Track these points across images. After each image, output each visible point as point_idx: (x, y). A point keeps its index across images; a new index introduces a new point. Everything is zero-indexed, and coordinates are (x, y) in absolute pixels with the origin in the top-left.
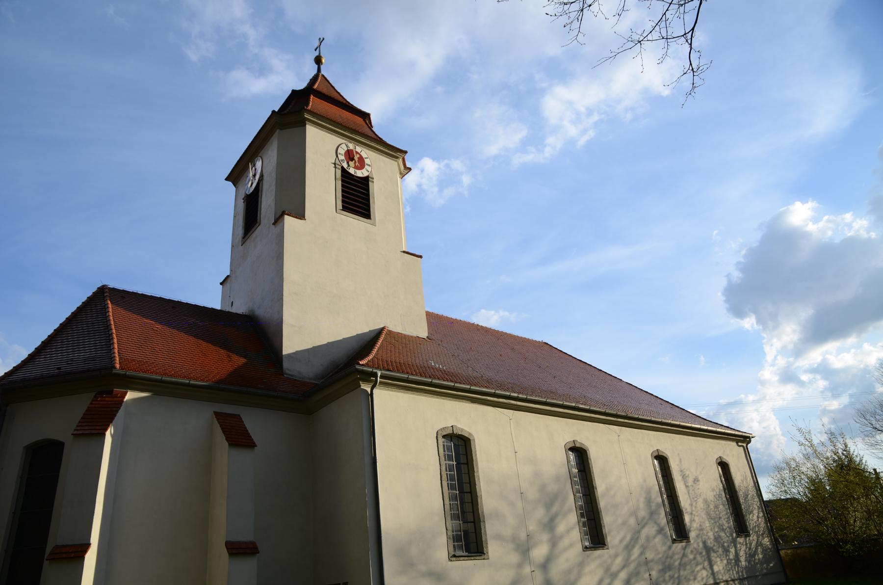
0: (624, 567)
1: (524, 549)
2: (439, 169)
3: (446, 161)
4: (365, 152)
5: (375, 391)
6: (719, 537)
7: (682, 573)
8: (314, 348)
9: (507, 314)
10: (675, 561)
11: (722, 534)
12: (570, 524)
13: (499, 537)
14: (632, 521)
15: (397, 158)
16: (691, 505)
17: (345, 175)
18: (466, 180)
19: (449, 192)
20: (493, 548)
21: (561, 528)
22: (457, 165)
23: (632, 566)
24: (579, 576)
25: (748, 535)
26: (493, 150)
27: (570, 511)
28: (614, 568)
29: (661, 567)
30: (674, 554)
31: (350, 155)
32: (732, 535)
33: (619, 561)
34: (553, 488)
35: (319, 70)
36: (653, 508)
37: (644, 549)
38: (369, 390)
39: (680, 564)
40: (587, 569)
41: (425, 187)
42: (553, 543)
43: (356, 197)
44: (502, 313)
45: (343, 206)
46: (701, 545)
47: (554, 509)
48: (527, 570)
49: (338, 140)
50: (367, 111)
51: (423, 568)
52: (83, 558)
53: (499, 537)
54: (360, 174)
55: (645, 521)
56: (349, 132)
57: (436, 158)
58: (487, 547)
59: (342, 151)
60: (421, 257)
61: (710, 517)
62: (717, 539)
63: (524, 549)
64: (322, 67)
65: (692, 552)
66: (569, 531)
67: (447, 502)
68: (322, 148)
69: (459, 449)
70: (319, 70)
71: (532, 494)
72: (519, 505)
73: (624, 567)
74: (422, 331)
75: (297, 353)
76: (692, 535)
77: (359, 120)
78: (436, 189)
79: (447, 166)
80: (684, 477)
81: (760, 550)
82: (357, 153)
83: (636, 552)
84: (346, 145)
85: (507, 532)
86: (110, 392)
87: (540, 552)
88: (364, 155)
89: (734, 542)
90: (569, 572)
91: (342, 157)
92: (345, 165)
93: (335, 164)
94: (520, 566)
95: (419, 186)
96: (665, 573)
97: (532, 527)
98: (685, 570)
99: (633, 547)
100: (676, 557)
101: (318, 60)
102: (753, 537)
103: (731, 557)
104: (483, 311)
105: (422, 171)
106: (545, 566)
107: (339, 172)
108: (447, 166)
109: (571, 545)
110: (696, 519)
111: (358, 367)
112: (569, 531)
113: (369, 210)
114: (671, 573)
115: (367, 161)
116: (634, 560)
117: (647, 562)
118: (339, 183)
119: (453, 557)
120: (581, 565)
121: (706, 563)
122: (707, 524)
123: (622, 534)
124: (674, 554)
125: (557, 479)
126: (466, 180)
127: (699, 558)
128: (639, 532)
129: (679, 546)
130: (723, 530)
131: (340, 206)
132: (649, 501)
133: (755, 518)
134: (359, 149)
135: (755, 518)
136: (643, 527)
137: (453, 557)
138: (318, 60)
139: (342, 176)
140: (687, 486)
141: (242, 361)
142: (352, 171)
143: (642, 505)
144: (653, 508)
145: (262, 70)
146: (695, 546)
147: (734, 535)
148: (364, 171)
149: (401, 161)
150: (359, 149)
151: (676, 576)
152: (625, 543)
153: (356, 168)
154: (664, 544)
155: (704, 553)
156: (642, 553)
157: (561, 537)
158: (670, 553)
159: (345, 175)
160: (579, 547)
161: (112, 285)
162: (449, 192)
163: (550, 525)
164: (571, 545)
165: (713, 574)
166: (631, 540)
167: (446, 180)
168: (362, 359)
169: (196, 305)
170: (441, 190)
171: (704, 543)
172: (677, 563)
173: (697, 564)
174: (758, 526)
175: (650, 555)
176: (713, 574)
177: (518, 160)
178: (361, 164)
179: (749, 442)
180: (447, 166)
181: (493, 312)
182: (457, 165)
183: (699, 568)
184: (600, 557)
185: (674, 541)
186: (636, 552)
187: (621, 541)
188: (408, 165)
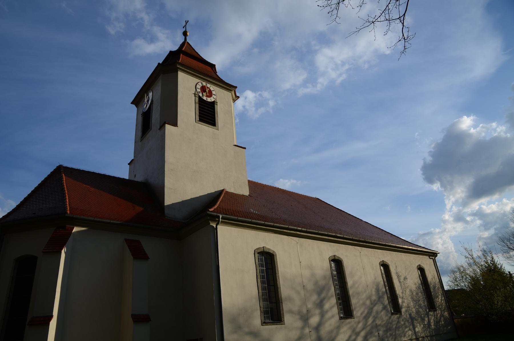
0: (363, 329)
1: (305, 318)
2: (255, 97)
3: (260, 92)
4: (212, 87)
7: (397, 332)
9: (295, 181)
11: (421, 310)
12: (332, 304)
13: (291, 312)
14: (368, 302)
15: (231, 90)
17: (200, 98)
18: (271, 103)
19: (262, 110)
20: (287, 318)
21: (327, 306)
22: (266, 94)
24: (337, 334)
26: (287, 86)
27: (332, 296)
28: (358, 330)
29: (385, 329)
30: (392, 321)
31: (203, 89)
32: (426, 310)
33: (360, 325)
34: (322, 283)
35: (185, 39)
38: (215, 226)
39: (396, 327)
41: (247, 107)
42: (322, 315)
43: (207, 114)
44: (292, 181)
45: (200, 119)
46: (408, 316)
47: (323, 295)
48: (307, 330)
49: (197, 80)
50: (214, 63)
51: (246, 330)
53: (291, 312)
54: (209, 100)
56: (203, 75)
57: (254, 90)
58: (284, 318)
59: (199, 86)
60: (245, 148)
61: (413, 300)
62: (418, 312)
63: (305, 318)
64: (187, 37)
65: (403, 320)
66: (331, 308)
68: (187, 85)
69: (267, 261)
70: (185, 39)
71: (310, 286)
72: (302, 292)
73: (363, 329)
74: (245, 191)
76: (403, 310)
77: (209, 68)
78: (254, 109)
80: (398, 277)
81: (442, 319)
82: (208, 88)
83: (370, 320)
85: (295, 309)
87: (314, 320)
88: (212, 89)
89: (427, 314)
90: (331, 332)
91: (199, 90)
92: (201, 95)
93: (195, 94)
94: (303, 328)
95: (244, 107)
97: (310, 305)
99: (369, 317)
100: (394, 323)
101: (185, 34)
102: (439, 312)
104: (281, 180)
105: (246, 98)
106: (317, 328)
107: (197, 99)
108: (260, 95)
109: (333, 316)
110: (406, 301)
111: (208, 212)
112: (331, 308)
114: (391, 332)
115: (214, 93)
117: (377, 326)
118: (197, 105)
119: (264, 323)
120: (338, 328)
123: (362, 309)
125: (325, 277)
126: (271, 103)
127: (407, 324)
128: (372, 308)
130: (421, 307)
131: (198, 119)
132: (378, 290)
133: (440, 300)
134: (209, 85)
135: (440, 300)
137: (264, 323)
139: (199, 101)
140: (400, 282)
141: (141, 209)
142: (205, 98)
146: (405, 316)
148: (212, 98)
149: (233, 92)
150: (209, 85)
152: (364, 315)
153: (207, 96)
154: (387, 315)
156: (374, 321)
157: (327, 312)
159: (201, 103)
160: (337, 317)
162: (262, 110)
163: (320, 305)
164: (333, 316)
165: (415, 333)
166: (368, 313)
167: (260, 103)
170: (257, 109)
172: (394, 327)
173: (406, 327)
174: (442, 305)
175: (378, 322)
177: (302, 92)
178: (210, 94)
179: (436, 256)
180: (260, 95)
181: (287, 181)
182: (266, 94)
183: (407, 330)
184: (349, 323)
185: (392, 314)
186: (370, 320)
187: (361, 314)
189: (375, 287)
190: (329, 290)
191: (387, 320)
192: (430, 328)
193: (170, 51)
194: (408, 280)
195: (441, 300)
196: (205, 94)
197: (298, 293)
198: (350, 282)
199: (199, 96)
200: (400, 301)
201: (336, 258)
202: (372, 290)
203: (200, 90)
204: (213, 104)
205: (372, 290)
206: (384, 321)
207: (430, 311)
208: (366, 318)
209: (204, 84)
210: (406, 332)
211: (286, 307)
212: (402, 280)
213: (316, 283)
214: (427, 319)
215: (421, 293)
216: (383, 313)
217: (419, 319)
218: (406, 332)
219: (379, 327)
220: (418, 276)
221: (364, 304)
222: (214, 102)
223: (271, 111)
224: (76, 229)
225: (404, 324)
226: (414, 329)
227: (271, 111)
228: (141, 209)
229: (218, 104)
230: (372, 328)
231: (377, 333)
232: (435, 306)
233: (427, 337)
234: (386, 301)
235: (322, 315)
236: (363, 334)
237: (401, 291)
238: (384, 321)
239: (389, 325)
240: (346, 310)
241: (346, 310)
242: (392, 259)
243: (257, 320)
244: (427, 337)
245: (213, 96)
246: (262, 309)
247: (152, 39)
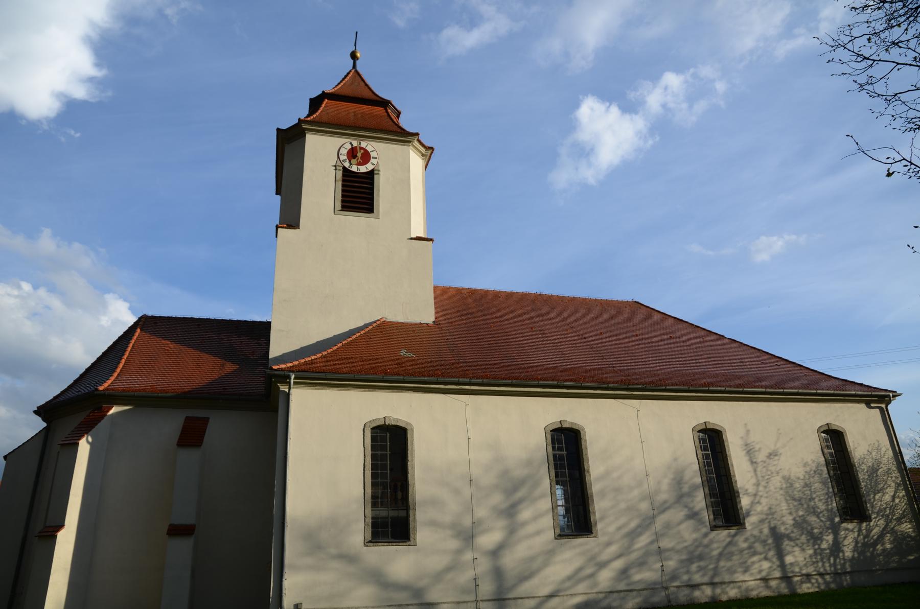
0: (619, 556)
1: (467, 536)
2: (686, 82)
3: (692, 70)
5: (292, 391)
6: (805, 521)
7: (722, 564)
8: (302, 348)
9: (794, 237)
10: (712, 550)
11: (812, 519)
12: (543, 508)
13: (433, 524)
14: (644, 506)
15: (409, 142)
18: (721, 87)
19: (701, 106)
20: (422, 534)
21: (525, 514)
22: (706, 71)
23: (634, 556)
24: (546, 564)
26: (748, 43)
27: (542, 496)
29: (684, 557)
30: (711, 542)
32: (832, 520)
33: (613, 549)
34: (519, 473)
37: (658, 537)
38: (287, 390)
39: (721, 554)
40: (558, 558)
42: (512, 531)
43: (358, 193)
44: (787, 237)
46: (766, 531)
47: (519, 495)
48: (468, 556)
51: (333, 551)
53: (433, 524)
54: (363, 169)
55: (668, 505)
56: (351, 130)
58: (415, 534)
59: (344, 151)
60: (431, 240)
62: (800, 524)
64: (357, 62)
65: (746, 540)
68: (323, 155)
72: (467, 492)
77: (379, 110)
78: (685, 106)
79: (694, 76)
80: (750, 452)
81: (888, 537)
83: (643, 540)
84: (343, 144)
85: (447, 519)
86: (100, 409)
87: (489, 539)
88: (369, 149)
89: (835, 530)
90: (532, 559)
91: (343, 158)
92: (347, 165)
94: (459, 552)
95: (664, 106)
96: (692, 563)
97: (481, 512)
98: (729, 559)
99: (640, 534)
100: (715, 545)
101: (353, 56)
102: (877, 525)
103: (824, 545)
104: (763, 238)
105: (666, 88)
106: (495, 553)
107: (340, 173)
109: (538, 533)
110: (764, 501)
113: (372, 204)
114: (702, 564)
115: (372, 154)
116: (638, 549)
117: (660, 551)
118: (340, 184)
119: (367, 543)
120: (550, 554)
121: (771, 554)
122: (784, 506)
123: (623, 520)
124: (711, 542)
125: (529, 463)
126: (721, 87)
127: (758, 547)
128: (653, 518)
132: (678, 481)
133: (887, 498)
134: (363, 144)
135: (888, 496)
136: (664, 511)
137: (367, 543)
138: (353, 56)
139: (343, 175)
142: (354, 168)
143: (665, 486)
144: (686, 489)
145: (472, 21)
146: (756, 532)
147: (837, 519)
149: (416, 143)
151: (711, 566)
152: (626, 530)
153: (359, 164)
154: (696, 530)
155: (770, 541)
157: (524, 524)
158: (706, 541)
160: (551, 534)
161: (151, 313)
162: (701, 106)
163: (510, 512)
164: (538, 533)
165: (782, 566)
166: (639, 526)
168: (101, 385)
169: (230, 321)
170: (691, 107)
171: (773, 530)
172: (715, 553)
173: (755, 553)
174: (893, 508)
175: (665, 543)
176: (782, 566)
177: (783, 49)
178: (366, 157)
179: (889, 402)
181: (775, 238)
182: (706, 71)
183: (755, 558)
184: (581, 545)
185: (714, 528)
186: (643, 540)
187: (619, 529)
188: (428, 144)
193: (311, 100)
196: (354, 161)
197: (457, 492)
199: (344, 168)
202: (659, 483)
203: (345, 157)
204: (370, 176)
205: (659, 483)
209: (355, 144)
210: (753, 563)
211: (421, 516)
213: (505, 473)
214: (830, 538)
215: (824, 483)
216: (683, 526)
217: (803, 538)
218: (753, 563)
219: (667, 554)
221: (629, 509)
222: (373, 171)
224: (114, 410)
225: (750, 547)
228: (235, 367)
229: (381, 173)
230: (647, 554)
231: (658, 565)
232: (866, 509)
233: (821, 575)
234: (700, 501)
235: (512, 531)
236: (618, 564)
237: (754, 481)
238: (685, 541)
239: (700, 549)
240: (578, 519)
241: (578, 519)
242: (733, 418)
244: (821, 575)
245: (372, 160)
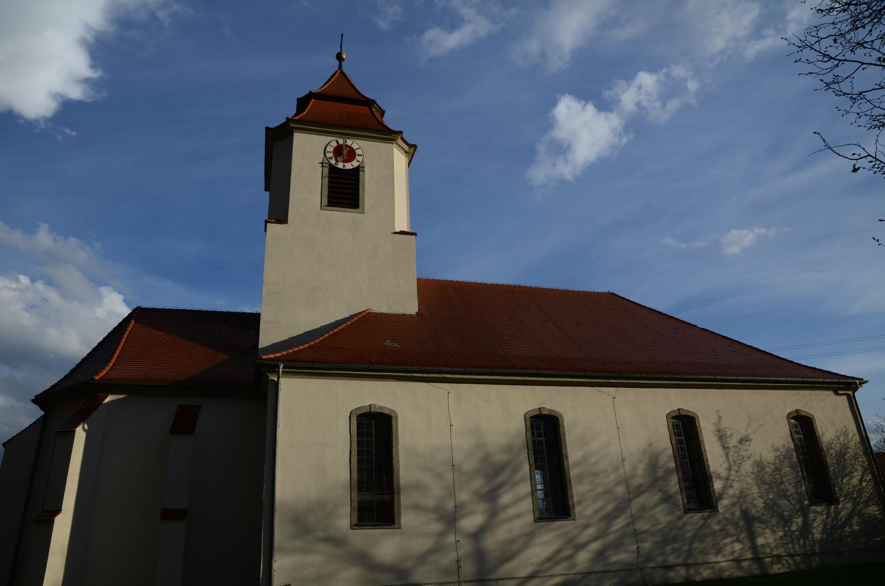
0: (596, 538)
1: (450, 519)
2: (659, 81)
3: (665, 70)
4: (353, 143)
6: (775, 504)
7: (696, 545)
8: (290, 338)
9: (763, 231)
11: (783, 502)
12: (521, 496)
14: (620, 490)
15: (393, 140)
16: (729, 469)
17: (333, 169)
18: (692, 86)
19: (674, 104)
20: (407, 518)
21: (506, 498)
22: (679, 71)
23: (611, 538)
24: (525, 546)
25: (836, 501)
26: (718, 43)
27: (522, 481)
30: (685, 524)
32: (802, 503)
35: (340, 67)
36: (660, 473)
37: (634, 519)
43: (344, 190)
44: (757, 231)
45: (329, 202)
46: (738, 514)
47: (500, 479)
49: (325, 139)
51: (321, 534)
52: (51, 522)
53: (417, 508)
54: (349, 166)
58: (399, 518)
59: (330, 149)
60: (415, 234)
61: (760, 480)
62: (771, 507)
63: (450, 519)
66: (516, 501)
67: (355, 475)
70: (340, 67)
71: (470, 465)
72: (449, 476)
73: (596, 538)
74: (411, 307)
75: (273, 345)
76: (723, 504)
78: (658, 104)
79: (667, 75)
80: (722, 437)
83: (619, 523)
84: (332, 142)
85: (431, 502)
87: (471, 522)
88: (355, 146)
90: (512, 541)
92: (333, 162)
94: (442, 535)
95: (638, 104)
97: (463, 496)
99: (616, 517)
100: (689, 528)
101: (339, 57)
102: (845, 507)
104: (734, 232)
105: (640, 87)
106: (477, 535)
107: (326, 170)
109: (518, 516)
110: (736, 485)
112: (516, 501)
113: (358, 200)
114: (676, 545)
115: (358, 152)
116: (615, 532)
117: (636, 534)
118: (326, 180)
122: (755, 490)
123: (600, 504)
124: (685, 524)
125: (509, 448)
126: (692, 86)
127: (731, 529)
128: (629, 501)
129: (696, 517)
130: (787, 498)
131: (325, 201)
132: (653, 465)
133: (855, 481)
137: (353, 526)
138: (339, 57)
139: (330, 172)
140: (725, 448)
142: (340, 165)
149: (400, 141)
153: (345, 161)
154: (670, 513)
156: (631, 523)
157: (505, 507)
158: (680, 523)
159: (333, 169)
160: (530, 518)
162: (674, 104)
163: (491, 496)
165: (754, 547)
166: (615, 510)
167: (670, 90)
170: (664, 105)
172: (689, 535)
174: (860, 491)
175: (641, 526)
176: (754, 547)
178: (351, 155)
181: (745, 231)
182: (679, 71)
183: (728, 540)
184: (559, 527)
185: (687, 511)
186: (619, 523)
187: (597, 511)
189: (646, 461)
190: (516, 469)
191: (669, 523)
192: (806, 539)
193: (298, 99)
194: (753, 443)
195: (861, 481)
196: (339, 158)
197: (440, 477)
198: (573, 453)
199: (331, 165)
200: (717, 485)
201: (544, 412)
203: (331, 155)
206: (660, 524)
207: (812, 503)
208: (609, 518)
209: (341, 141)
210: (726, 545)
212: (733, 442)
213: (486, 459)
215: (792, 467)
218: (726, 545)
220: (788, 433)
222: (358, 167)
223: (694, 101)
225: (722, 530)
226: (752, 537)
227: (694, 101)
231: (634, 547)
233: (791, 556)
234: (674, 485)
235: (493, 514)
236: (595, 546)
237: (726, 465)
239: (674, 531)
240: (556, 502)
241: (556, 502)
243: (343, 520)
244: (791, 556)
245: (357, 158)
246: (356, 505)
247: (453, 23)
